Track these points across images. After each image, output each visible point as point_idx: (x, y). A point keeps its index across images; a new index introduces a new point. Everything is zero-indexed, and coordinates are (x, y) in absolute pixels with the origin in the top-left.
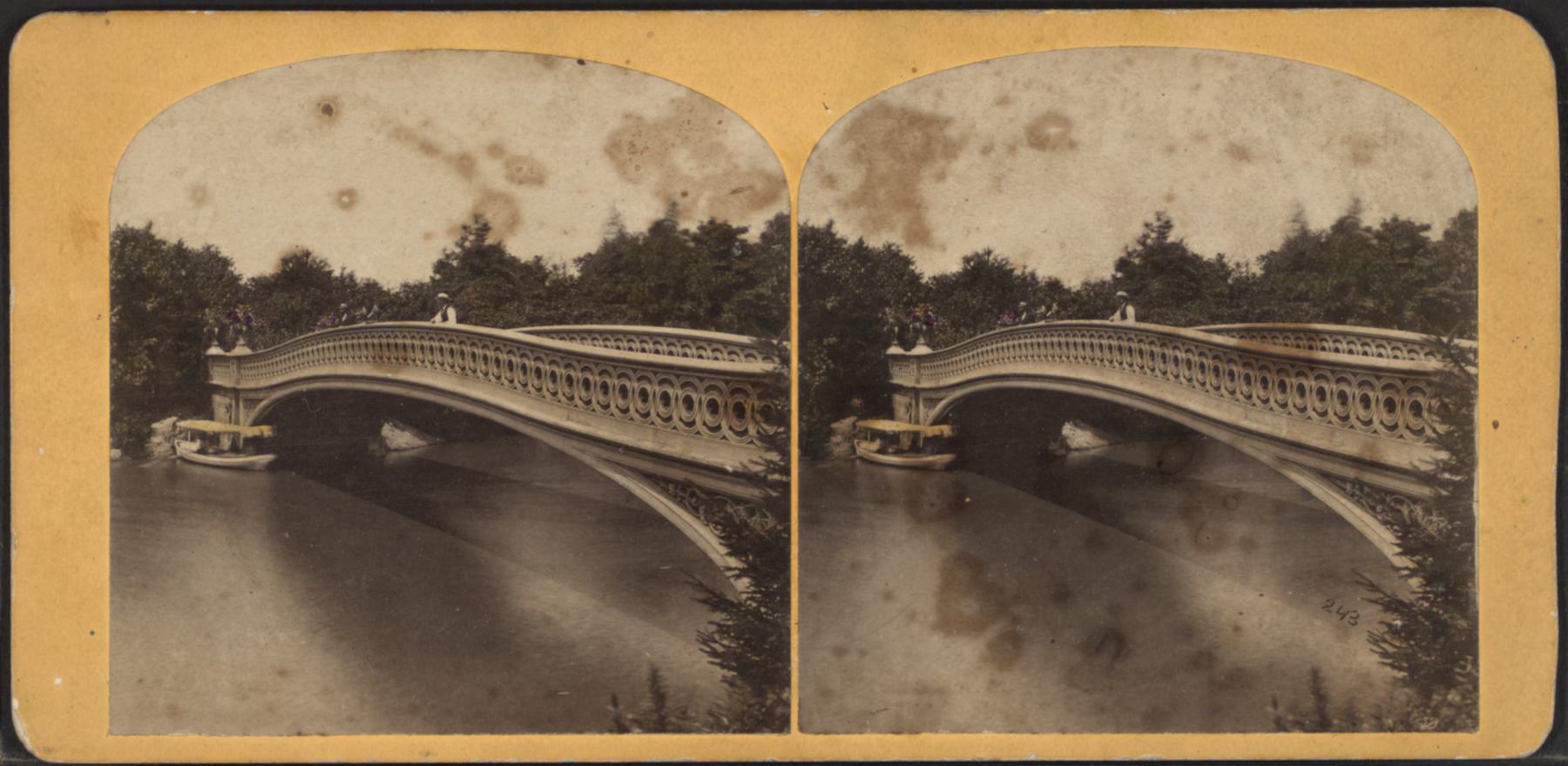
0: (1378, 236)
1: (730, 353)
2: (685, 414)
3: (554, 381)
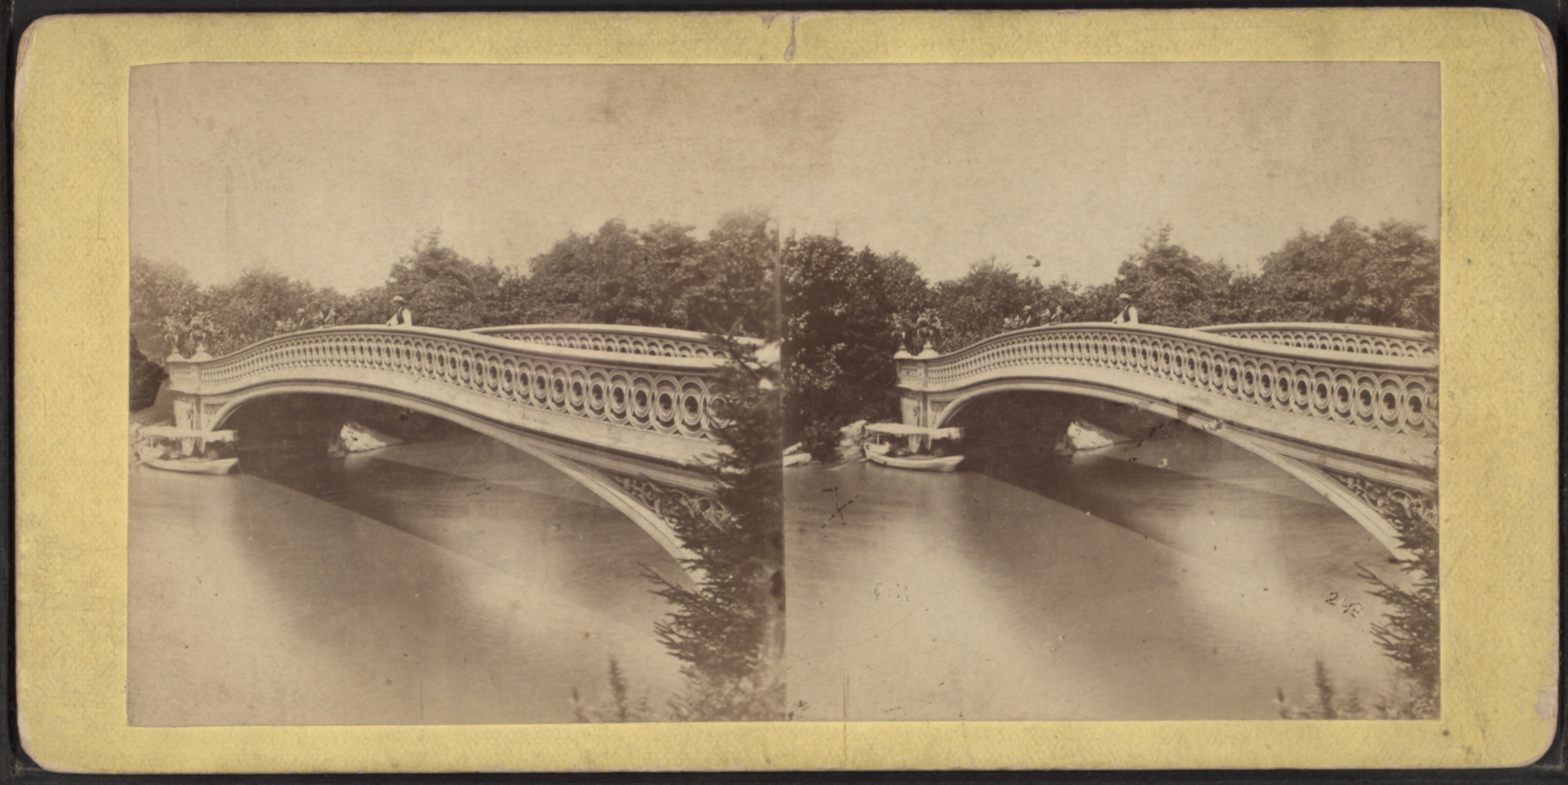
0: (1377, 236)
1: (698, 351)
2: (638, 410)
3: (509, 380)
